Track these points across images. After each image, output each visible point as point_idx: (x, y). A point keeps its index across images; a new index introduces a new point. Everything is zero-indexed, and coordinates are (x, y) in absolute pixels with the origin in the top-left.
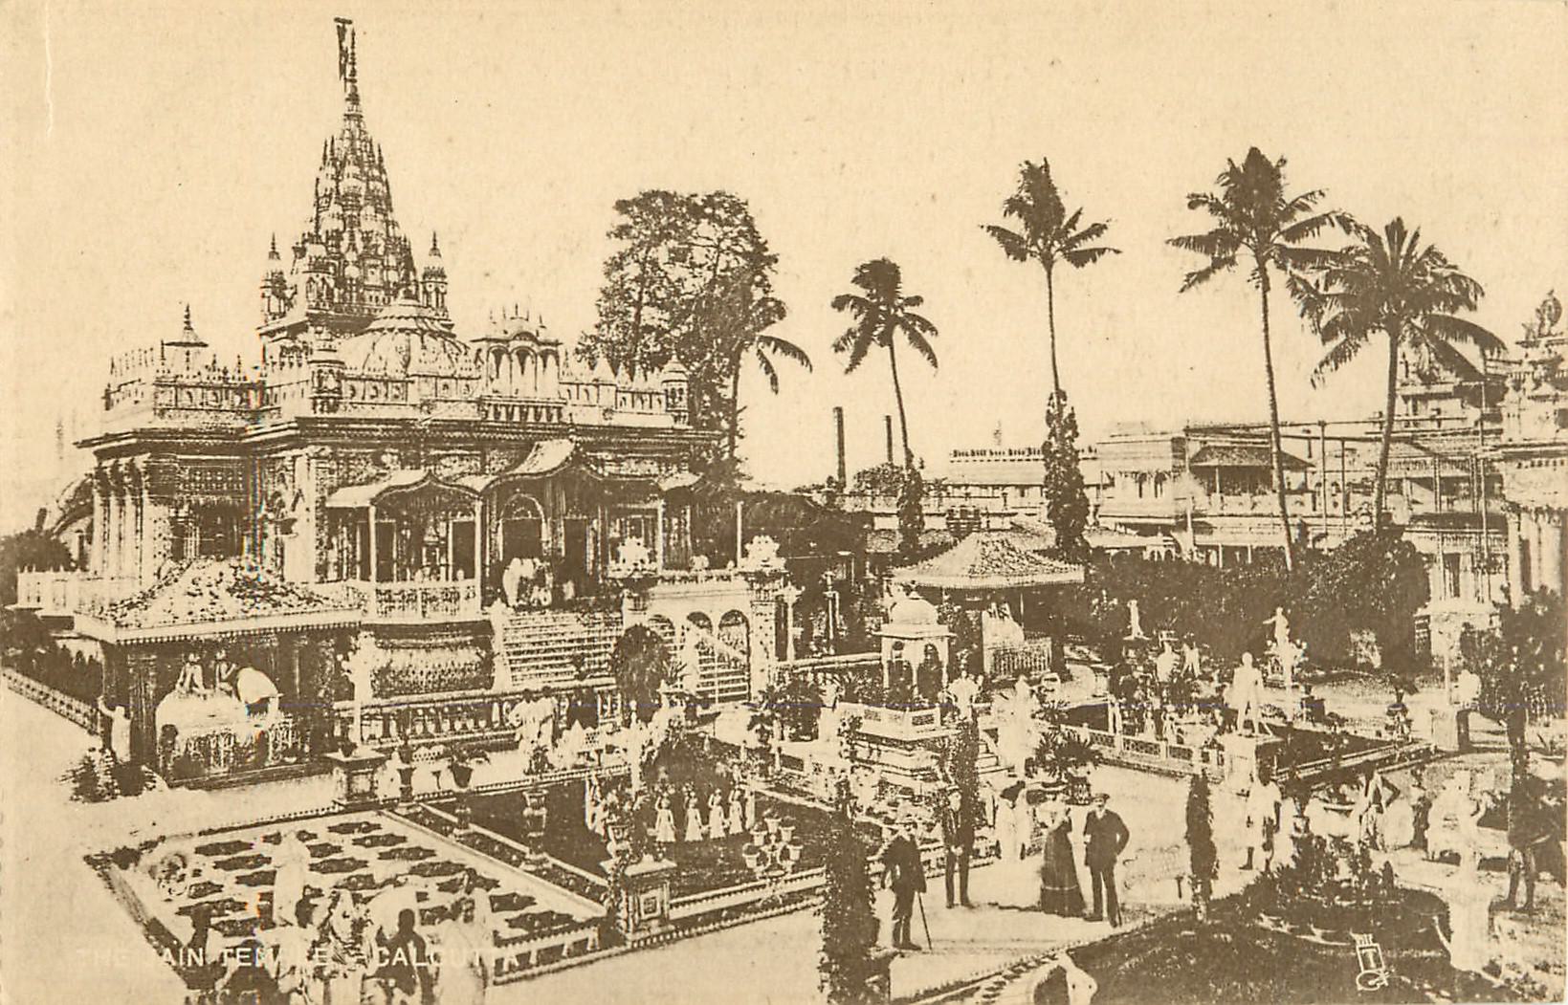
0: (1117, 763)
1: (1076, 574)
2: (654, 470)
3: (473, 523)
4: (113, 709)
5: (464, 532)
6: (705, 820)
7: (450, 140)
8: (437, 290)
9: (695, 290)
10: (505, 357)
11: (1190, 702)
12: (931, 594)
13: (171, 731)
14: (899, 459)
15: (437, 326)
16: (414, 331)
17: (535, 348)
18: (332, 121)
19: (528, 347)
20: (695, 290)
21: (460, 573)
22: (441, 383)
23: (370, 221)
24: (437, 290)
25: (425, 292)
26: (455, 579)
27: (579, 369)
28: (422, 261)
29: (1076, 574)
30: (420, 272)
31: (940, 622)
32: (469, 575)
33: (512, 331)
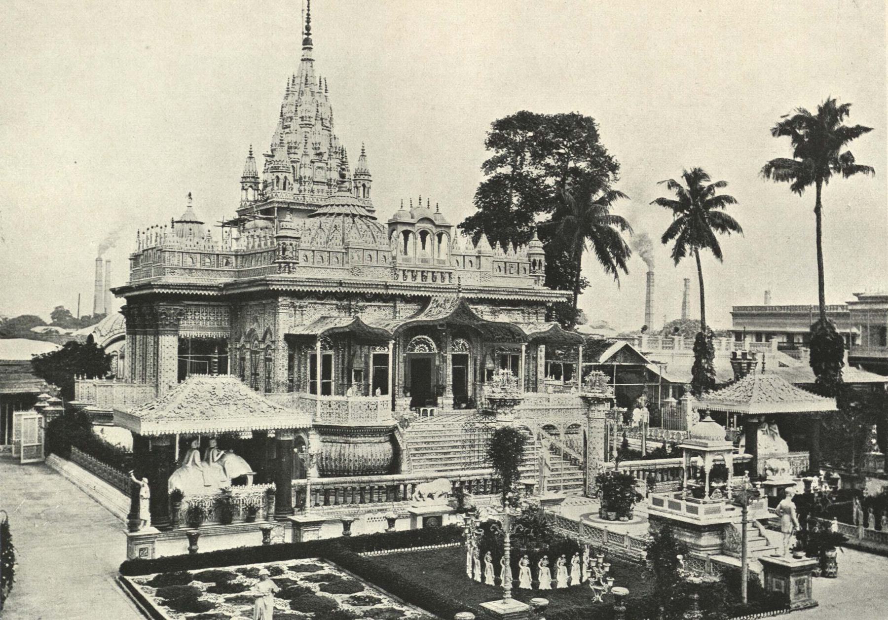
0: (859, 548)
1: (829, 405)
2: (520, 320)
3: (387, 355)
4: (141, 480)
5: (381, 360)
6: (553, 574)
7: (147, 48)
8: (364, 185)
9: (549, 186)
10: (411, 235)
11: (72, 411)
12: (720, 417)
13: (178, 496)
14: (694, 314)
15: (364, 212)
16: (347, 215)
17: (435, 230)
18: (291, 65)
19: (430, 228)
20: (549, 186)
21: (378, 391)
22: (367, 253)
23: (318, 136)
24: (364, 185)
25: (357, 187)
26: (374, 394)
27: (464, 242)
28: (353, 165)
29: (829, 405)
30: (352, 172)
31: (727, 439)
32: (384, 392)
33: (418, 215)
